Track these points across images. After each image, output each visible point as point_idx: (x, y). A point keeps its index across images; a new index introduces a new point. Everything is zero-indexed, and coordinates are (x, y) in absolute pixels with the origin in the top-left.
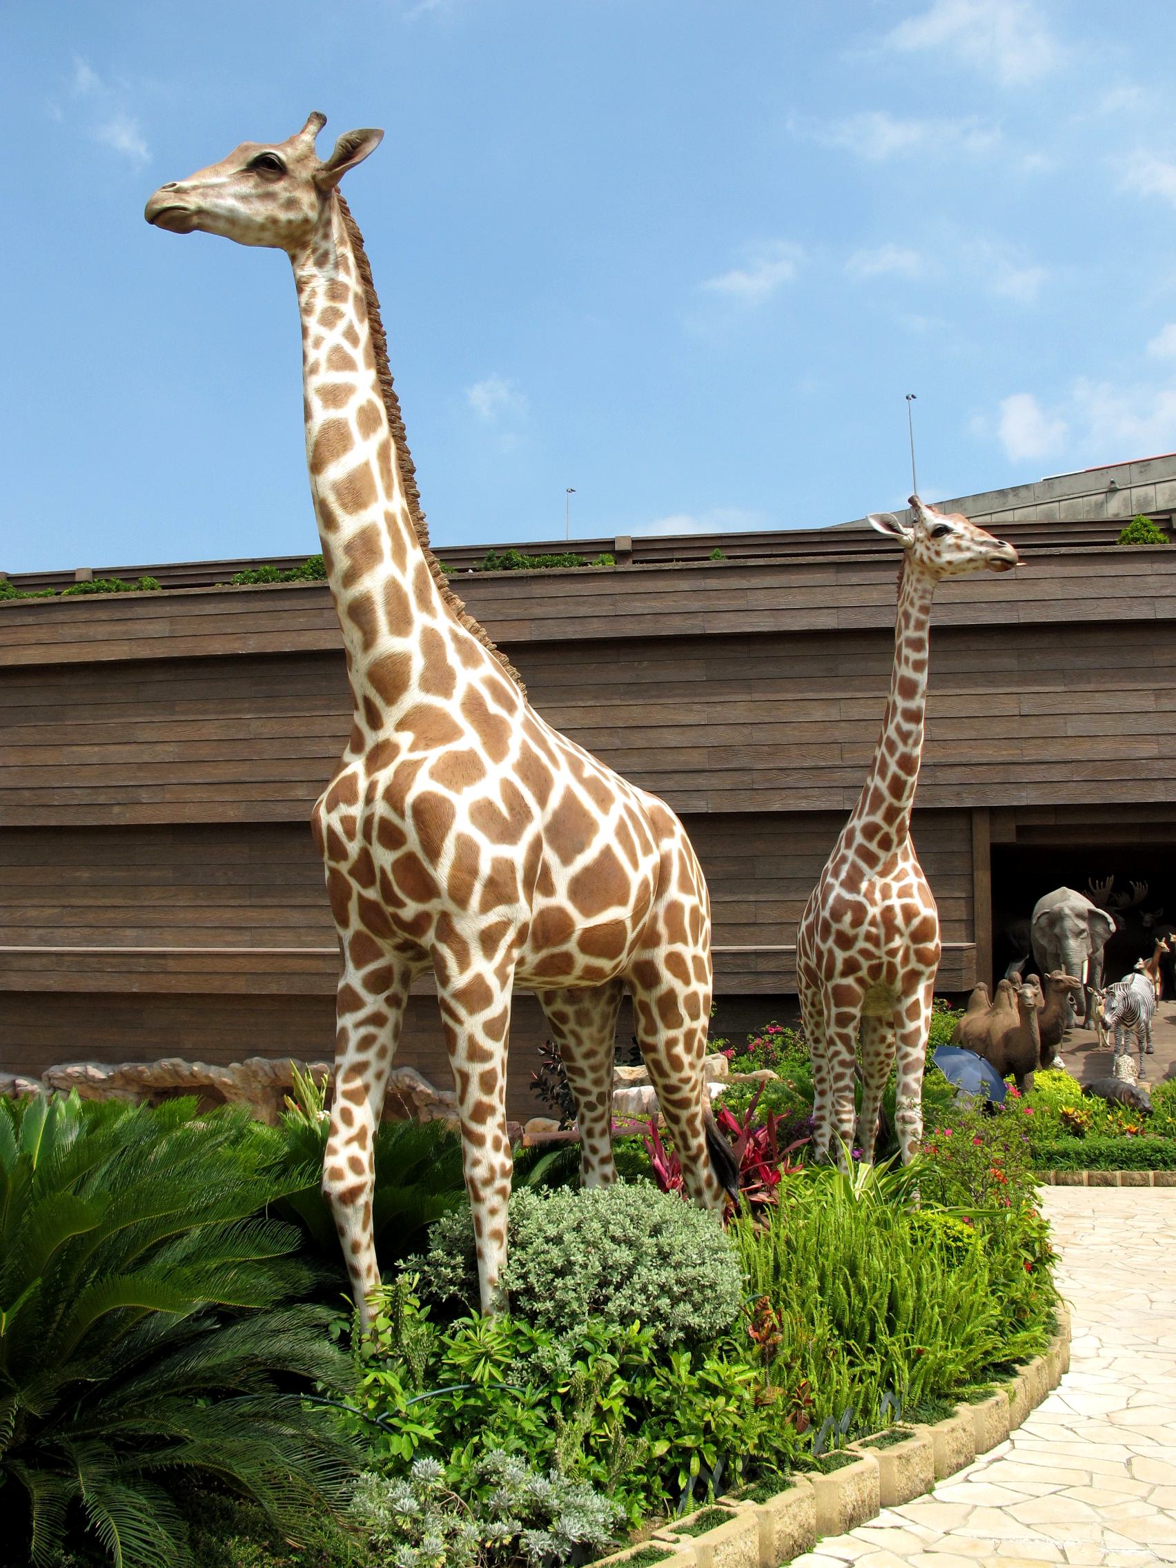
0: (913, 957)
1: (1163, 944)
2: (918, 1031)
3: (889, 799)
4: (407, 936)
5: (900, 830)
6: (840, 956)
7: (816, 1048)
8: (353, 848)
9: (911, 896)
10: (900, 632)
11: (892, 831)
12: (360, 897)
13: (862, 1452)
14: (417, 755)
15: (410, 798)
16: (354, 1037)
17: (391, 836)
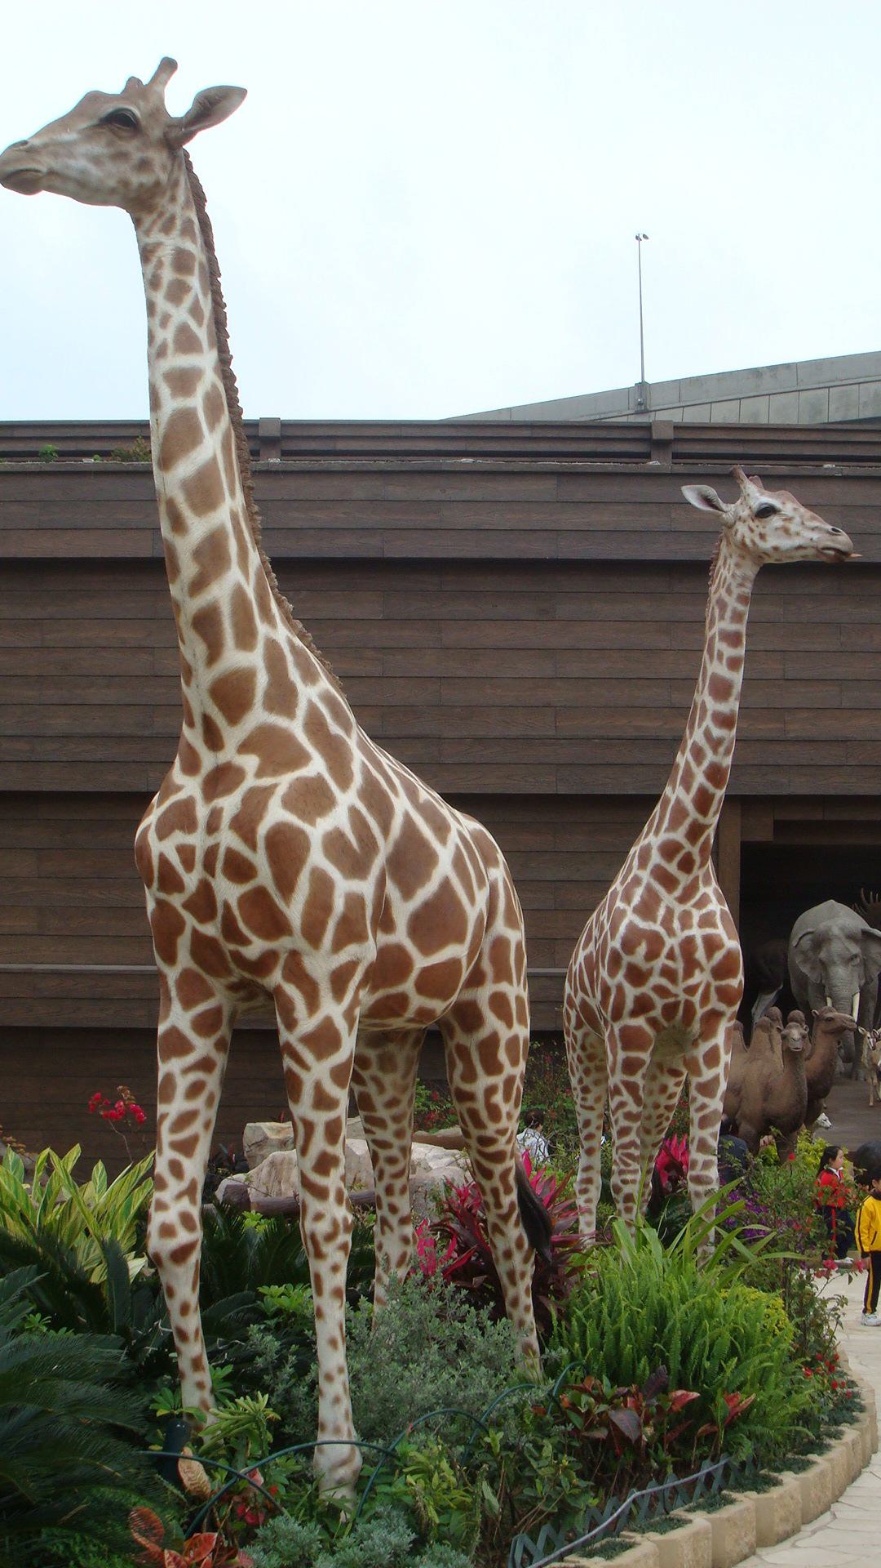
0: (713, 996)
2: (716, 1079)
3: (693, 814)
4: (247, 975)
5: (703, 850)
6: (631, 992)
7: (584, 1099)
8: (191, 881)
9: (714, 926)
10: (712, 623)
11: (695, 851)
12: (195, 932)
13: (690, 1516)
14: (266, 781)
15: (263, 829)
16: (182, 1083)
17: (239, 869)
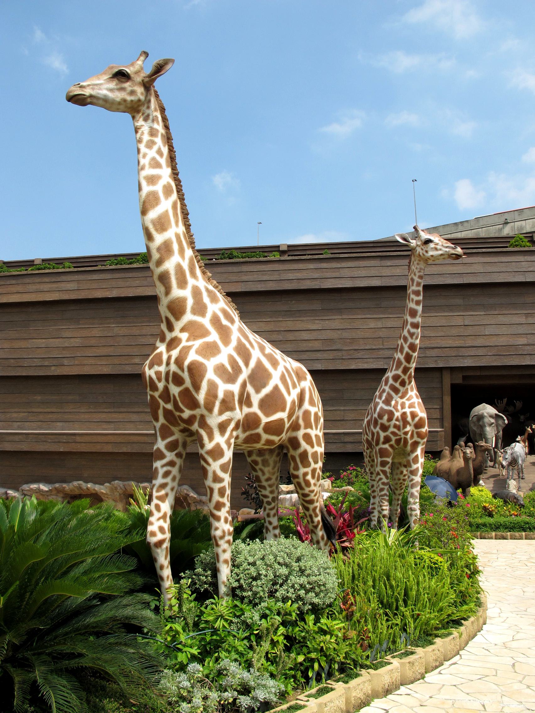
0: (415, 435)
1: (529, 429)
2: (417, 469)
3: (404, 363)
4: (185, 425)
5: (410, 377)
6: (382, 435)
7: (371, 477)
8: (161, 386)
9: (414, 407)
10: (409, 287)
11: (406, 378)
12: (164, 408)
13: (392, 660)
14: (190, 343)
15: (186, 363)
16: (161, 471)
17: (178, 380)
